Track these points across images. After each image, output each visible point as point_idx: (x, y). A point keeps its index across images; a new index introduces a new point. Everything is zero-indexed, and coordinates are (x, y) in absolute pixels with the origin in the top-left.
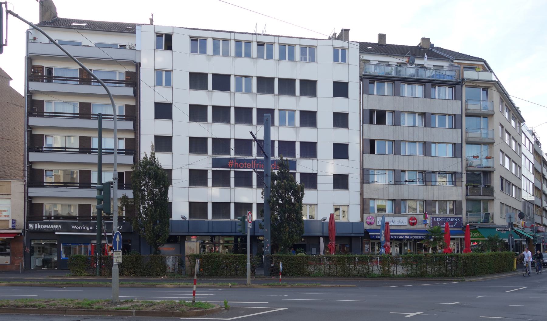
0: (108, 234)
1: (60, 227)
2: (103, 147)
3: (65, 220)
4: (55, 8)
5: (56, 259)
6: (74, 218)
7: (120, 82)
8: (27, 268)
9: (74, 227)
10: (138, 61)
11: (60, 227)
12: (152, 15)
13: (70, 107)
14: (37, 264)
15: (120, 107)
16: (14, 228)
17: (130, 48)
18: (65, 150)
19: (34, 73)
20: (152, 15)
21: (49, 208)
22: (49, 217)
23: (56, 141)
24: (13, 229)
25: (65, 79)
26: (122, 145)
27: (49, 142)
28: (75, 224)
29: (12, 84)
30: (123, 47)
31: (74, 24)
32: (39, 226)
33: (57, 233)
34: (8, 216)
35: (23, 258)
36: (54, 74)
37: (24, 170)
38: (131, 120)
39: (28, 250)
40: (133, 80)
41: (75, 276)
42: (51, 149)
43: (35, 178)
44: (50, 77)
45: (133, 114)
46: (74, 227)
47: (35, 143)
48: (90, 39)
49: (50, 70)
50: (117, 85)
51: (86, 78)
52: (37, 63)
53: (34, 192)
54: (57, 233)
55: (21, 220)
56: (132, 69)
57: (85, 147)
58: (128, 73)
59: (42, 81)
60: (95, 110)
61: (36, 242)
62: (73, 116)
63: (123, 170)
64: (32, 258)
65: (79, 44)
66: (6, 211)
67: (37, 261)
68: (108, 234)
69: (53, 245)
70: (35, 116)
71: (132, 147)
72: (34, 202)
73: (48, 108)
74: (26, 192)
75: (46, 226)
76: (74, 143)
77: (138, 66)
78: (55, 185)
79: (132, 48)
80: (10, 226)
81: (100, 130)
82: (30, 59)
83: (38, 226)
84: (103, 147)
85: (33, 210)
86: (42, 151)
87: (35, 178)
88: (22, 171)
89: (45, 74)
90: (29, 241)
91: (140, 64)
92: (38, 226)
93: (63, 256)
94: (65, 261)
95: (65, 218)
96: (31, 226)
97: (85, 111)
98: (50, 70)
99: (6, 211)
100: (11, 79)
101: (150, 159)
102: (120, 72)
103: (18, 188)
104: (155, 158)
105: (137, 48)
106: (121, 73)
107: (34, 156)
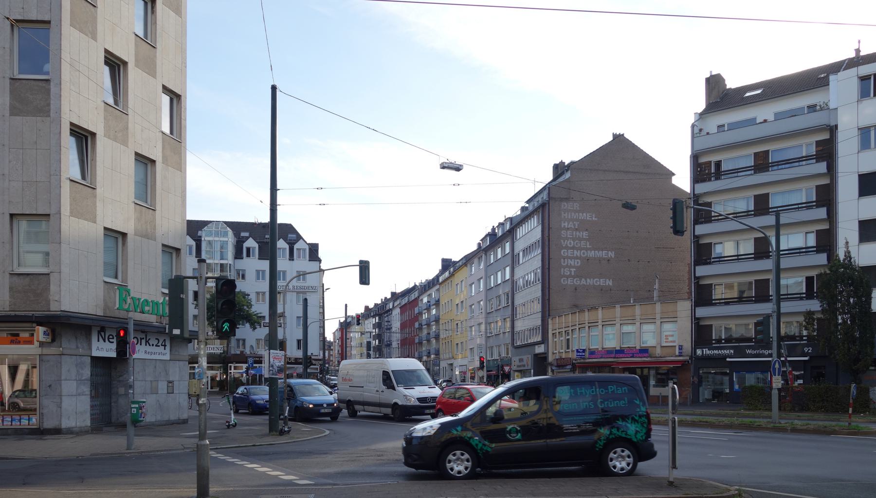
0: (789, 359)
1: (732, 351)
2: (781, 248)
3: (738, 343)
4: (724, 80)
5: (727, 391)
6: (749, 340)
7: (808, 158)
8: (695, 401)
9: (748, 351)
10: (833, 124)
11: (732, 351)
12: (859, 42)
13: (744, 203)
14: (706, 397)
15: (804, 193)
16: (680, 355)
17: (822, 109)
18: (738, 258)
19: (701, 170)
20: (859, 42)
21: (719, 331)
22: (719, 341)
23: (726, 248)
24: (680, 356)
25: (736, 171)
26: (812, 241)
27: (718, 250)
28: (749, 347)
29: (675, 181)
30: (812, 108)
31: (748, 94)
32: (708, 352)
33: (728, 359)
34: (674, 342)
35: (690, 389)
36: (724, 167)
37: (12, 51)
38: (823, 206)
39: (696, 379)
40: (827, 152)
41: (750, 410)
42: (721, 259)
43: (703, 295)
44: (719, 173)
45: (826, 197)
46: (748, 351)
47: (703, 253)
48: (765, 112)
49: (718, 164)
50: (804, 163)
51: (762, 163)
52: (703, 160)
53: (701, 312)
54: (728, 359)
55: (688, 346)
56: (825, 136)
57: (762, 250)
58: (818, 143)
59: (710, 180)
60: (774, 202)
61: (705, 370)
62: (747, 214)
63: (813, 273)
64: (701, 389)
65: (752, 122)
66: (672, 336)
67: (705, 393)
68: (789, 359)
69: (725, 374)
70: (701, 223)
71: (826, 241)
72: (702, 323)
73: (717, 209)
74: (693, 312)
75: (716, 352)
76: (748, 247)
77: (833, 130)
78: (727, 302)
79: (825, 108)
80: (677, 353)
81: (778, 227)
82: (695, 158)
83: (707, 352)
84: (781, 248)
85: (701, 333)
86: (710, 263)
87: (703, 295)
88: (685, 286)
89: (713, 170)
90: (697, 370)
91: (836, 126)
92: (707, 352)
93: (736, 387)
94: (737, 392)
95: (739, 340)
96: (699, 352)
97: (762, 206)
98: (718, 164)
99: (672, 336)
100: (674, 174)
101: (844, 260)
102: (807, 146)
103: (684, 308)
104: (851, 259)
105: (832, 106)
106: (808, 145)
107: (701, 271)
